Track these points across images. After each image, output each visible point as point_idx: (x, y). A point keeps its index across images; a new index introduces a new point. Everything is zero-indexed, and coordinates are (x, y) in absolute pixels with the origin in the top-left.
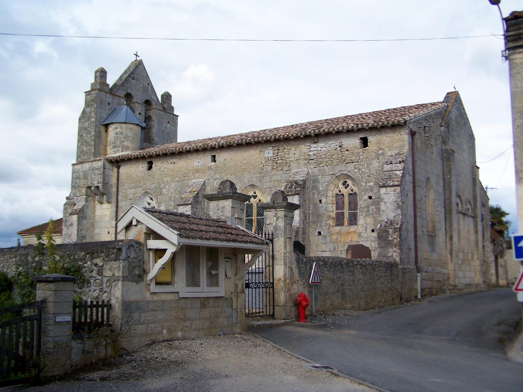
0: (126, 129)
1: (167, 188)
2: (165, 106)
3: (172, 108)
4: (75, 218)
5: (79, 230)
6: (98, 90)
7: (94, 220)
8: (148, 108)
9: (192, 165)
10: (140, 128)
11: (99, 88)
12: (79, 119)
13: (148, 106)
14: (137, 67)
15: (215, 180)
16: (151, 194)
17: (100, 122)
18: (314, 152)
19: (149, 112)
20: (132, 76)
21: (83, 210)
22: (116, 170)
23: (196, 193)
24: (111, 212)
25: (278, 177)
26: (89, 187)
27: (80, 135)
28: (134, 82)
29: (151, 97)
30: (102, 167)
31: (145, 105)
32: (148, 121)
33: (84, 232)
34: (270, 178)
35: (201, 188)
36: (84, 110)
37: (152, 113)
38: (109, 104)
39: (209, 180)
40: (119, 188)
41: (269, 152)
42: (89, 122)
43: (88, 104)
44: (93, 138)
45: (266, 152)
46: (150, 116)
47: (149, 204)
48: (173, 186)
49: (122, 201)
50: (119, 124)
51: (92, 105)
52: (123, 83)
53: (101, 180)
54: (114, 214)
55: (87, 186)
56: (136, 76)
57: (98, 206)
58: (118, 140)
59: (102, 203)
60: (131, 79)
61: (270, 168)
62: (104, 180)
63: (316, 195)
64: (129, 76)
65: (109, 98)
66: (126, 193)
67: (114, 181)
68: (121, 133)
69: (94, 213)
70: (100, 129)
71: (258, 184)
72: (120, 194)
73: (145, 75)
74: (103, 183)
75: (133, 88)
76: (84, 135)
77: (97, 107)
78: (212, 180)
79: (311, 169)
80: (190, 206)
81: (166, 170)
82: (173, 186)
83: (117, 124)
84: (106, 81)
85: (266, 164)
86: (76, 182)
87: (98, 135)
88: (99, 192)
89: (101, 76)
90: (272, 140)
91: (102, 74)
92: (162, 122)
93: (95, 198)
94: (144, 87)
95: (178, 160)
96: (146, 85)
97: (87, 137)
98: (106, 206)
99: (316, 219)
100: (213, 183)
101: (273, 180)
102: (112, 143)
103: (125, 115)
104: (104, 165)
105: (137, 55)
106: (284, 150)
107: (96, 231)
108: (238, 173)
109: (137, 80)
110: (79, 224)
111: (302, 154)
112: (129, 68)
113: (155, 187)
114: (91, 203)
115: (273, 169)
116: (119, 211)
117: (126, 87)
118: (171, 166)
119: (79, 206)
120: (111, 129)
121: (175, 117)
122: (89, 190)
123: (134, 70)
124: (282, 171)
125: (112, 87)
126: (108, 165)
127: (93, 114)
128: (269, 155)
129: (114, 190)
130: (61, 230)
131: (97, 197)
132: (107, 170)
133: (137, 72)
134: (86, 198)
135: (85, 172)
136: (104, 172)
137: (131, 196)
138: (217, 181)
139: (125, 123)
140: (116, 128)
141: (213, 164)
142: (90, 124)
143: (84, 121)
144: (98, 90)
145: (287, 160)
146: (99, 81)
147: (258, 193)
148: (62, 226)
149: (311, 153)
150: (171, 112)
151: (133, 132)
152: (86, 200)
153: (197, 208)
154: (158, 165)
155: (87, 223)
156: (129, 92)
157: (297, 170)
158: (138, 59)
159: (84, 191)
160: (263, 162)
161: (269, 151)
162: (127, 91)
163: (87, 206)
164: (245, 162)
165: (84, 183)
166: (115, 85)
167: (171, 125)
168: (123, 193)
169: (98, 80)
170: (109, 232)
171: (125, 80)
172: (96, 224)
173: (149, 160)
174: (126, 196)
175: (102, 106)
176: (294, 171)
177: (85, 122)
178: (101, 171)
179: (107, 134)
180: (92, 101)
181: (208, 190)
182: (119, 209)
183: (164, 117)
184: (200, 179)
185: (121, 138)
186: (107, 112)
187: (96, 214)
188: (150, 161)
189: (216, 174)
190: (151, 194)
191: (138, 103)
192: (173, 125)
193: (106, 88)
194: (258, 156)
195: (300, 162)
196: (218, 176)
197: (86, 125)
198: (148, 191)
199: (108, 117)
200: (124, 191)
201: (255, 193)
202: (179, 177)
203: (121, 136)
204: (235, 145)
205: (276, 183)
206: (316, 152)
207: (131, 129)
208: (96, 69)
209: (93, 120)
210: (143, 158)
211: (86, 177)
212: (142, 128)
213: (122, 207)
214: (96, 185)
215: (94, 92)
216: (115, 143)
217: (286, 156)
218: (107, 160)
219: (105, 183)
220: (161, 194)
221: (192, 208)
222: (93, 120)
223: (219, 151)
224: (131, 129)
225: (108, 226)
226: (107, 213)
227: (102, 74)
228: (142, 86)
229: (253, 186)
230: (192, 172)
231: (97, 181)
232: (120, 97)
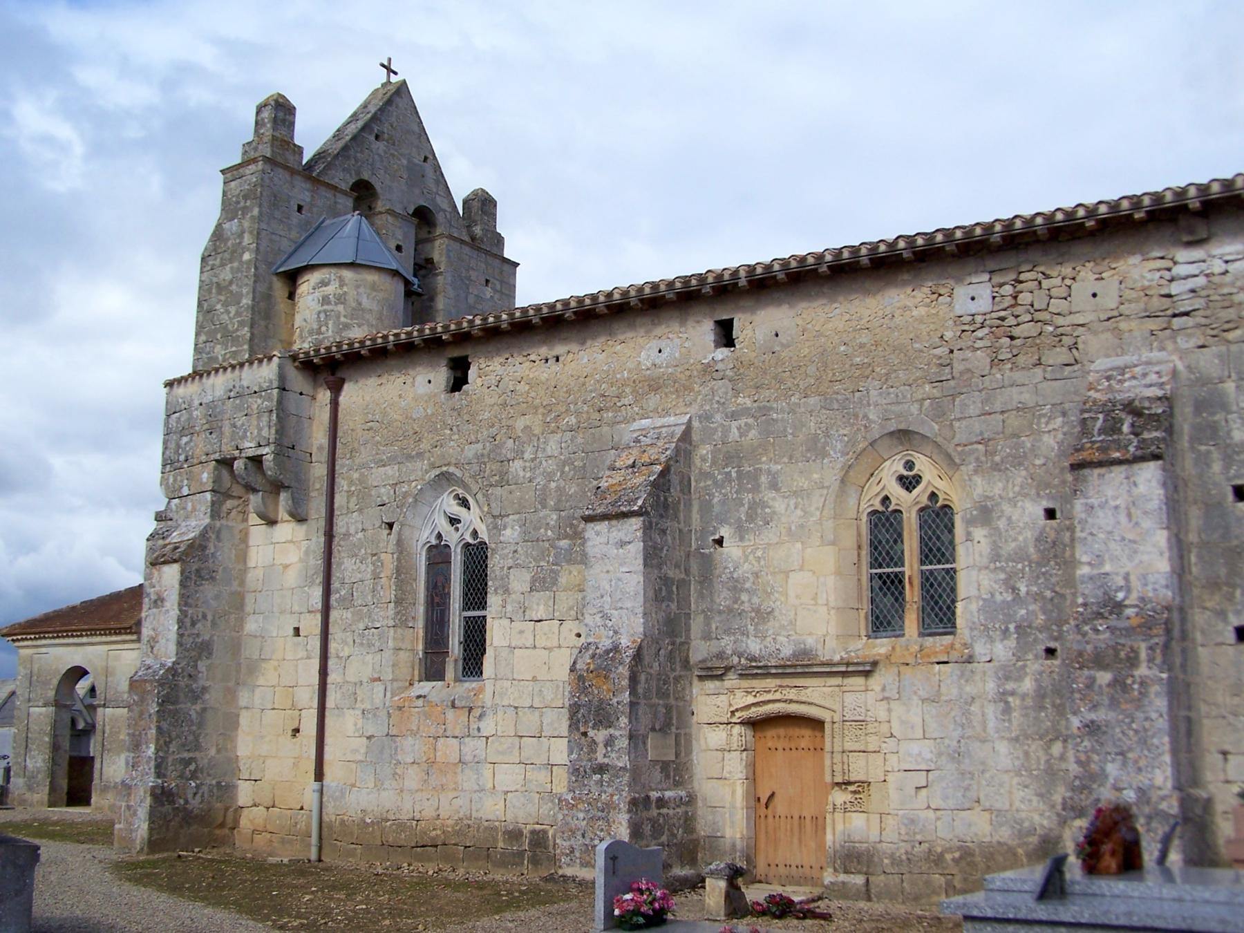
0: (358, 287)
1: (527, 456)
2: (478, 230)
3: (499, 241)
4: (171, 574)
5: (188, 621)
6: (266, 160)
7: (242, 583)
8: (423, 235)
9: (630, 365)
10: (401, 287)
11: (268, 155)
12: (203, 259)
13: (426, 229)
14: (389, 102)
15: (734, 416)
16: (466, 487)
17: (270, 264)
18: (1191, 284)
19: (428, 246)
20: (376, 128)
21: (204, 548)
22: (325, 396)
23: (658, 468)
24: (307, 553)
25: (1027, 397)
27: (205, 310)
28: (380, 146)
29: (433, 200)
30: (275, 384)
31: (416, 221)
32: (424, 277)
33: (204, 631)
34: (985, 401)
35: (677, 449)
36: (219, 226)
37: (439, 251)
38: (300, 209)
39: (706, 417)
40: (339, 463)
41: (974, 294)
42: (236, 264)
43: (230, 208)
44: (247, 316)
45: (962, 292)
46: (430, 261)
47: (454, 521)
48: (552, 447)
50: (333, 270)
51: (245, 210)
52: (345, 148)
53: (269, 433)
54: (317, 562)
55: (217, 456)
56: (386, 128)
57: (257, 531)
58: (330, 323)
59: (272, 522)
60: (372, 138)
61: (981, 359)
62: (281, 431)
63: (1217, 467)
64: (366, 128)
65: (301, 192)
67: (318, 437)
68: (341, 299)
69: (243, 557)
70: (270, 288)
71: (931, 428)
72: (342, 484)
73: (416, 129)
74: (278, 443)
75: (378, 165)
76: (219, 307)
77: (261, 213)
78: (718, 417)
79: (1183, 354)
80: (636, 523)
81: (522, 387)
82: (552, 447)
83: (325, 270)
84: (292, 138)
85: (961, 344)
86: (178, 446)
88: (260, 479)
89: (275, 120)
90: (996, 238)
91: (280, 112)
92: (469, 278)
94: (411, 167)
95: (574, 347)
96: (418, 160)
97: (229, 316)
98: (287, 530)
99: (1223, 572)
100: (727, 430)
101: (998, 407)
103: (353, 241)
104: (282, 377)
105: (390, 71)
106: (1045, 284)
107: (251, 626)
108: (837, 387)
109: (392, 142)
110: (185, 600)
111: (1133, 295)
112: (365, 106)
113: (479, 457)
114: (234, 522)
115: (996, 362)
117: (357, 161)
118: (545, 373)
119: (187, 530)
120: (307, 285)
121: (506, 267)
123: (382, 110)
124: (1038, 371)
125: (311, 160)
126: (298, 381)
127: (247, 239)
128: (973, 307)
129: (319, 470)
130: (139, 623)
131: (255, 500)
132: (292, 397)
133: (390, 117)
134: (213, 503)
135: (211, 406)
137: (385, 493)
138: (742, 422)
139: (352, 265)
140: (324, 283)
141: (723, 352)
142: (238, 270)
143: (218, 262)
144: (266, 160)
145: (1060, 321)
146: (269, 133)
147: (923, 466)
148: (141, 610)
149: (1175, 289)
150: (495, 251)
151: (381, 295)
152: (215, 513)
153: (664, 532)
154: (488, 371)
155: (217, 597)
156: (366, 176)
157: (1119, 361)
158: (394, 79)
159: (206, 476)
160: (948, 335)
161: (971, 290)
162: (358, 173)
163: (218, 533)
164: (864, 338)
165: (209, 448)
166: (319, 156)
167: (495, 291)
168: (351, 483)
169: (267, 131)
170: (297, 631)
171: (354, 138)
172: (249, 599)
173: (456, 353)
174: (363, 495)
175: (277, 214)
176: (1102, 364)
177: (223, 265)
178: (269, 399)
179: (294, 305)
180: (246, 198)
181: (704, 460)
182: (336, 540)
183: (473, 264)
184: (668, 414)
185: (338, 317)
186: (294, 234)
187: (251, 564)
188: (456, 354)
189: (737, 393)
190: (466, 487)
191: (391, 212)
192: (501, 292)
193: (290, 157)
194: (922, 311)
195: (1123, 325)
196: (749, 403)
197: (226, 274)
198: (452, 469)
199: (295, 251)
200: (356, 476)
201: (909, 465)
202: (578, 413)
203: (340, 308)
204: (824, 269)
205: (1014, 421)
206: (1201, 281)
207: (374, 287)
208: (260, 100)
209: (246, 256)
210: (434, 344)
212: (409, 293)
213: (347, 535)
214: (251, 453)
215: (252, 168)
216: (319, 332)
217: (1056, 306)
218: (294, 358)
219: (287, 445)
220: (503, 481)
221: (647, 528)
222: (246, 256)
223: (747, 303)
224: (374, 287)
225: (296, 608)
226: (293, 556)
227: (281, 115)
228: (405, 162)
229: (904, 436)
230: (634, 391)
231: (254, 436)
232: (335, 188)
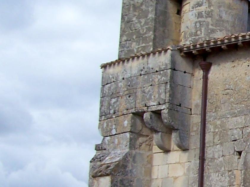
0: (220, 7)
21: (125, 167)
24: (188, 170)
26: (139, 115)
27: (126, 21)
30: (169, 66)
40: (208, 115)
44: (152, 25)
49: (215, 144)
53: (165, 96)
55: (133, 111)
57: (158, 157)
59: (167, 151)
62: (172, 95)
66: (222, 125)
68: (209, 14)
69: (149, 172)
70: (166, 7)
72: (210, 128)
74: (171, 102)
76: (134, 19)
86: (110, 104)
87: (161, 18)
93: (151, 139)
98: (176, 156)
102: (191, 35)
104: (173, 62)
114: (143, 151)
116: (206, 167)
119: (115, 156)
122: (138, 121)
126: (183, 64)
129: (196, 119)
132: (179, 75)
134: (131, 139)
136: (172, 77)
151: (234, 12)
152: (132, 145)
159: (126, 123)
163: (134, 158)
168: (216, 127)
174: (223, 134)
178: (165, 75)
179: (181, 18)
182: (206, 162)
185: (208, 25)
187: (154, 176)
200: (219, 122)
203: (209, 20)
211: (131, 92)
213: (213, 159)
214: (154, 109)
216: (196, 35)
218: (181, 50)
226: (180, 172)
231: (156, 98)
